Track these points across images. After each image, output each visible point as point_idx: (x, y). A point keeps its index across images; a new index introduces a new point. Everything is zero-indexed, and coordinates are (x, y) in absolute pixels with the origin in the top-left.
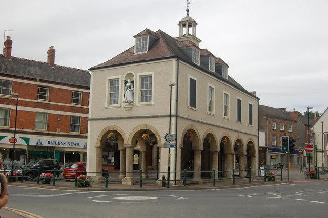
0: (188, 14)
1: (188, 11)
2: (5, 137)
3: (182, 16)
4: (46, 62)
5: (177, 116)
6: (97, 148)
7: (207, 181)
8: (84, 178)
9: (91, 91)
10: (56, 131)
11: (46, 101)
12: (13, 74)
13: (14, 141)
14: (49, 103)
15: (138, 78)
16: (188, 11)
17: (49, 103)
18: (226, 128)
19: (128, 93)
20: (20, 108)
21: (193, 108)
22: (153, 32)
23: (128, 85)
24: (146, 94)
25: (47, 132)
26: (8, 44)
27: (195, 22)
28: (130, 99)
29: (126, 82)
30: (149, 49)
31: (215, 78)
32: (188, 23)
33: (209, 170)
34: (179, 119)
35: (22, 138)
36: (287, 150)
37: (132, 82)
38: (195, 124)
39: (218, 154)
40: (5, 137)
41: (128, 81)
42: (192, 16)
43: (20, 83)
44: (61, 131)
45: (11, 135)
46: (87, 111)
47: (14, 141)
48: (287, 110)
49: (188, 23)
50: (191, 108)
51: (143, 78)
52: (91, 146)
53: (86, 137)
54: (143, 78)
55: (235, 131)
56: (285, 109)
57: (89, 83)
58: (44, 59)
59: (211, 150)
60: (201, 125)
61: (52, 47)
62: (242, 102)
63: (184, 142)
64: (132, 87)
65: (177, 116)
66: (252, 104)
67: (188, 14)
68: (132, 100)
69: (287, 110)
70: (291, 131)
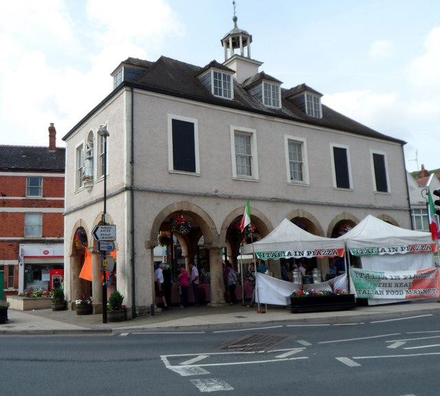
0: (236, 25)
1: (235, 19)
3: (228, 28)
7: (402, 241)
11: (40, 197)
12: (44, 168)
16: (235, 19)
17: (44, 198)
21: (189, 173)
26: (52, 131)
32: (238, 39)
34: (136, 194)
38: (193, 201)
42: (242, 26)
43: (53, 178)
48: (324, 101)
49: (238, 39)
50: (379, 193)
52: (64, 251)
53: (62, 242)
56: (321, 95)
57: (64, 164)
58: (45, 143)
60: (213, 201)
65: (131, 189)
67: (236, 25)
69: (324, 101)
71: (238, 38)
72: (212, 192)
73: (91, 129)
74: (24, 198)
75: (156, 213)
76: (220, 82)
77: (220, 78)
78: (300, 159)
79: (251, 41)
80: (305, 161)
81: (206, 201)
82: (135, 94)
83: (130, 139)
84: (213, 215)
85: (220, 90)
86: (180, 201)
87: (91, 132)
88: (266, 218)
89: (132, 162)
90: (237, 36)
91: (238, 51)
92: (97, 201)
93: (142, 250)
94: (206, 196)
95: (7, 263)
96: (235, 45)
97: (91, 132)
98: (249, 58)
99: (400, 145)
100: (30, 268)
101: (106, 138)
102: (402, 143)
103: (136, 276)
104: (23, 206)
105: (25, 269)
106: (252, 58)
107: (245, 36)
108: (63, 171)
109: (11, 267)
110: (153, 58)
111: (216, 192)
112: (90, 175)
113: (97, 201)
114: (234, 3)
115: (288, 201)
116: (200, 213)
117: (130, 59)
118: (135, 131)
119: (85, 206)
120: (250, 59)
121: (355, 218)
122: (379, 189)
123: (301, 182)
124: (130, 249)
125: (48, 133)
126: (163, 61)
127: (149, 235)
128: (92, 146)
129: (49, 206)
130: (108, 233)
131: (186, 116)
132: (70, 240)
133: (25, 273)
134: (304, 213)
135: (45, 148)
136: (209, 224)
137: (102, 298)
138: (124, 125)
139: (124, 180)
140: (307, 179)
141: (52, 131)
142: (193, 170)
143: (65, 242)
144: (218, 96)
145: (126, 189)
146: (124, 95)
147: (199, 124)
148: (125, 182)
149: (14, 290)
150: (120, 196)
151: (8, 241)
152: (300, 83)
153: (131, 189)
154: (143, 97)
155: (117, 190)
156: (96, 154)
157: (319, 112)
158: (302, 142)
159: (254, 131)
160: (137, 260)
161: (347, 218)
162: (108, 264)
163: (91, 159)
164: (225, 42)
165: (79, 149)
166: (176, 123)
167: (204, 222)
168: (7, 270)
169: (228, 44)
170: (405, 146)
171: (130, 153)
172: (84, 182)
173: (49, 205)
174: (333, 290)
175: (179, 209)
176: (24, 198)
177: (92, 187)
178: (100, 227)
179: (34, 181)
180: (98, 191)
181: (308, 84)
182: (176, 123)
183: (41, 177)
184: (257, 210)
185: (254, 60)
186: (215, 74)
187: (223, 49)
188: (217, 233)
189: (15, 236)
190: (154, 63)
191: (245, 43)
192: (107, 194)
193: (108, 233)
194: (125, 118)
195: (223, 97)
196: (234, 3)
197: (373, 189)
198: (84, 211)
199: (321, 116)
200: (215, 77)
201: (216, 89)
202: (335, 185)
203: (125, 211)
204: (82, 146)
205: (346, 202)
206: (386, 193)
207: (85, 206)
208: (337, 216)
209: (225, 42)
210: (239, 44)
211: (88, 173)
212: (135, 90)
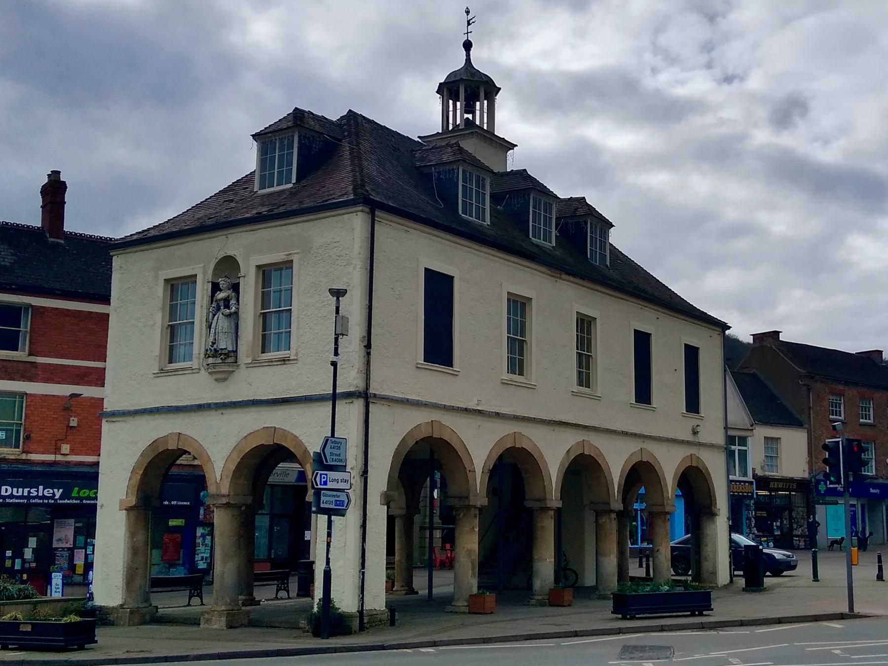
1: (468, 45)
4: (38, 224)
5: (366, 396)
6: (129, 510)
8: (436, 567)
10: (57, 451)
14: (32, 359)
15: (253, 271)
16: (468, 45)
17: (32, 359)
18: (585, 428)
19: (222, 322)
22: (322, 120)
23: (221, 295)
25: (24, 457)
28: (224, 343)
29: (216, 288)
30: (298, 180)
36: (831, 483)
37: (236, 288)
38: (450, 421)
39: (552, 513)
41: (222, 282)
42: (482, 61)
44: (73, 452)
46: (98, 378)
50: (430, 366)
51: (265, 272)
54: (265, 272)
55: (625, 434)
61: (56, 173)
64: (233, 302)
66: (693, 343)
68: (235, 349)
70: (871, 421)
183: (28, 307)
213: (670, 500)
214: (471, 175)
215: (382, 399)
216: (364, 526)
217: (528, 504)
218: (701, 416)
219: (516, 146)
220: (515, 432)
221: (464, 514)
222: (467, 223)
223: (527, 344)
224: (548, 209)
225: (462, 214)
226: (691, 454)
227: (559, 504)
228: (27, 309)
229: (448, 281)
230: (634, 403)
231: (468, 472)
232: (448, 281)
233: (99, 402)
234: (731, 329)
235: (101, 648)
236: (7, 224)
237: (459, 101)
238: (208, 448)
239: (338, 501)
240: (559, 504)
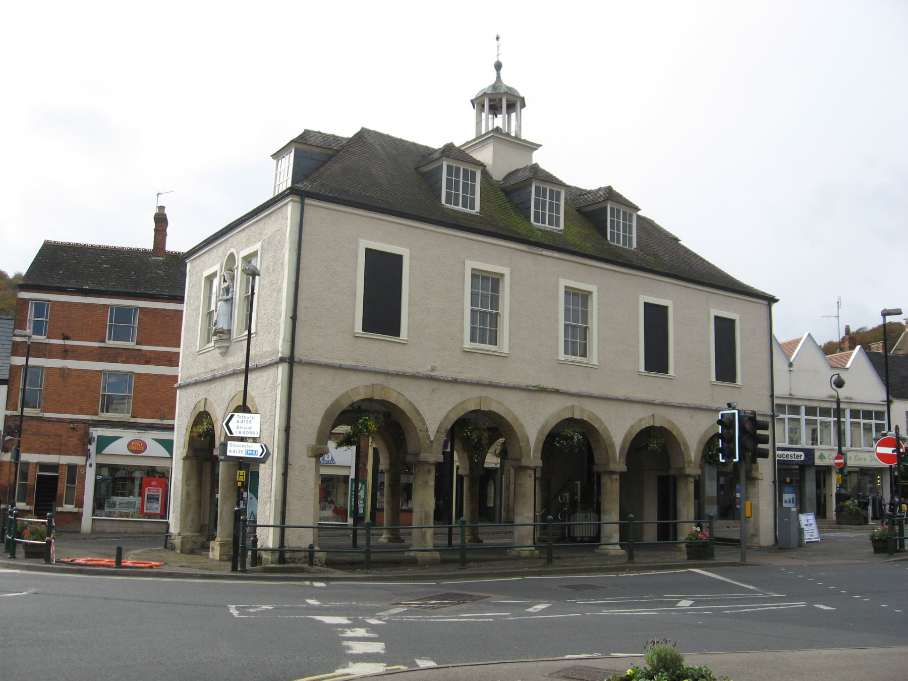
0: (498, 77)
1: (498, 66)
2: (153, 439)
3: (486, 81)
9: (185, 307)
11: (131, 345)
13: (137, 448)
16: (498, 66)
17: (138, 347)
20: (33, 361)
24: (483, 331)
26: (161, 221)
27: (523, 99)
31: (556, 255)
33: (676, 519)
34: (297, 369)
35: (157, 440)
38: (393, 383)
40: (153, 439)
42: (509, 80)
45: (128, 435)
46: (172, 360)
47: (137, 448)
50: (719, 383)
58: (147, 244)
59: (596, 469)
60: (427, 386)
62: (500, 298)
63: (192, 442)
65: (291, 361)
67: (498, 77)
71: (501, 100)
72: (424, 370)
73: (233, 250)
74: (102, 345)
75: (329, 401)
76: (457, 183)
77: (457, 176)
78: (585, 320)
79: (523, 105)
80: (594, 323)
81: (415, 384)
82: (306, 207)
83: (294, 280)
84: (423, 408)
85: (457, 196)
86: (369, 384)
87: (232, 257)
88: (514, 416)
89: (294, 318)
90: (499, 96)
91: (499, 121)
92: (234, 374)
93: (302, 460)
94: (414, 377)
95: (65, 460)
96: (495, 109)
97: (232, 255)
98: (517, 138)
99: (766, 302)
100: (105, 472)
101: (254, 279)
102: (771, 300)
103: (288, 499)
104: (100, 360)
105: (97, 474)
106: (524, 136)
107: (511, 98)
108: (181, 300)
109: (72, 468)
110: (347, 131)
111: (433, 369)
112: (226, 328)
113: (234, 374)
114: (498, 38)
115: (557, 392)
116: (402, 405)
117: (307, 133)
118: (301, 266)
119: (213, 379)
120: (520, 139)
121: (673, 424)
122: (719, 377)
123: (582, 359)
124: (282, 455)
125: (153, 225)
126: (363, 136)
127: (315, 436)
128: (232, 278)
129: (147, 362)
130: (248, 425)
131: (389, 243)
132: (184, 432)
133: (96, 481)
134: (582, 411)
135: (145, 252)
136: (418, 425)
137: (677, 496)
138: (287, 256)
139: (281, 347)
140: (594, 357)
141: (161, 221)
142: (395, 331)
143: (176, 427)
144: (452, 206)
145: (282, 360)
146: (290, 210)
147: (412, 258)
148: (280, 349)
149: (76, 510)
150: (271, 372)
151: (70, 421)
152: (604, 185)
153: (291, 361)
154: (318, 211)
155: (268, 361)
156: (238, 292)
157: (631, 238)
158: (591, 293)
159: (506, 271)
160: (291, 474)
161: (657, 424)
162: (250, 440)
163: (230, 301)
164: (477, 103)
165: (210, 279)
166: (372, 255)
167: (408, 419)
168: (63, 475)
169: (483, 106)
170: (775, 307)
171: (291, 306)
172: (215, 338)
173: (147, 359)
174: (248, 533)
175: (368, 396)
176: (102, 345)
177: (228, 347)
178: (236, 414)
179: (124, 314)
180: (237, 360)
181: (617, 189)
182: (372, 255)
183: (136, 308)
184: (502, 404)
185: (525, 141)
186: (449, 168)
187: (473, 112)
188: (429, 437)
189: (81, 412)
190: (350, 139)
191: (511, 107)
192: (251, 364)
193: (248, 425)
194: (287, 246)
195: (460, 208)
196: (498, 38)
197: (710, 377)
198: (212, 386)
199: (635, 245)
200: (449, 173)
201: (448, 195)
202: (642, 368)
203: (279, 394)
204: (214, 275)
205: (659, 399)
206: (732, 385)
207: (213, 379)
208: (641, 420)
209: (477, 103)
210: (501, 107)
211: (222, 325)
212: (307, 201)
213: (692, 463)
214: (618, 211)
215: (309, 364)
216: (285, 475)
217: (409, 458)
218: (669, 375)
219: (541, 146)
220: (480, 397)
221: (418, 470)
222: (545, 232)
223: (589, 329)
224: (555, 196)
225: (446, 203)
226: (573, 405)
227: (623, 468)
228: (136, 310)
229: (732, 322)
230: (644, 371)
231: (418, 431)
232: (732, 322)
233: (175, 378)
234: (779, 302)
235: (714, 560)
236: (130, 249)
237: (484, 112)
238: (188, 407)
239: (250, 451)
240: (623, 468)
